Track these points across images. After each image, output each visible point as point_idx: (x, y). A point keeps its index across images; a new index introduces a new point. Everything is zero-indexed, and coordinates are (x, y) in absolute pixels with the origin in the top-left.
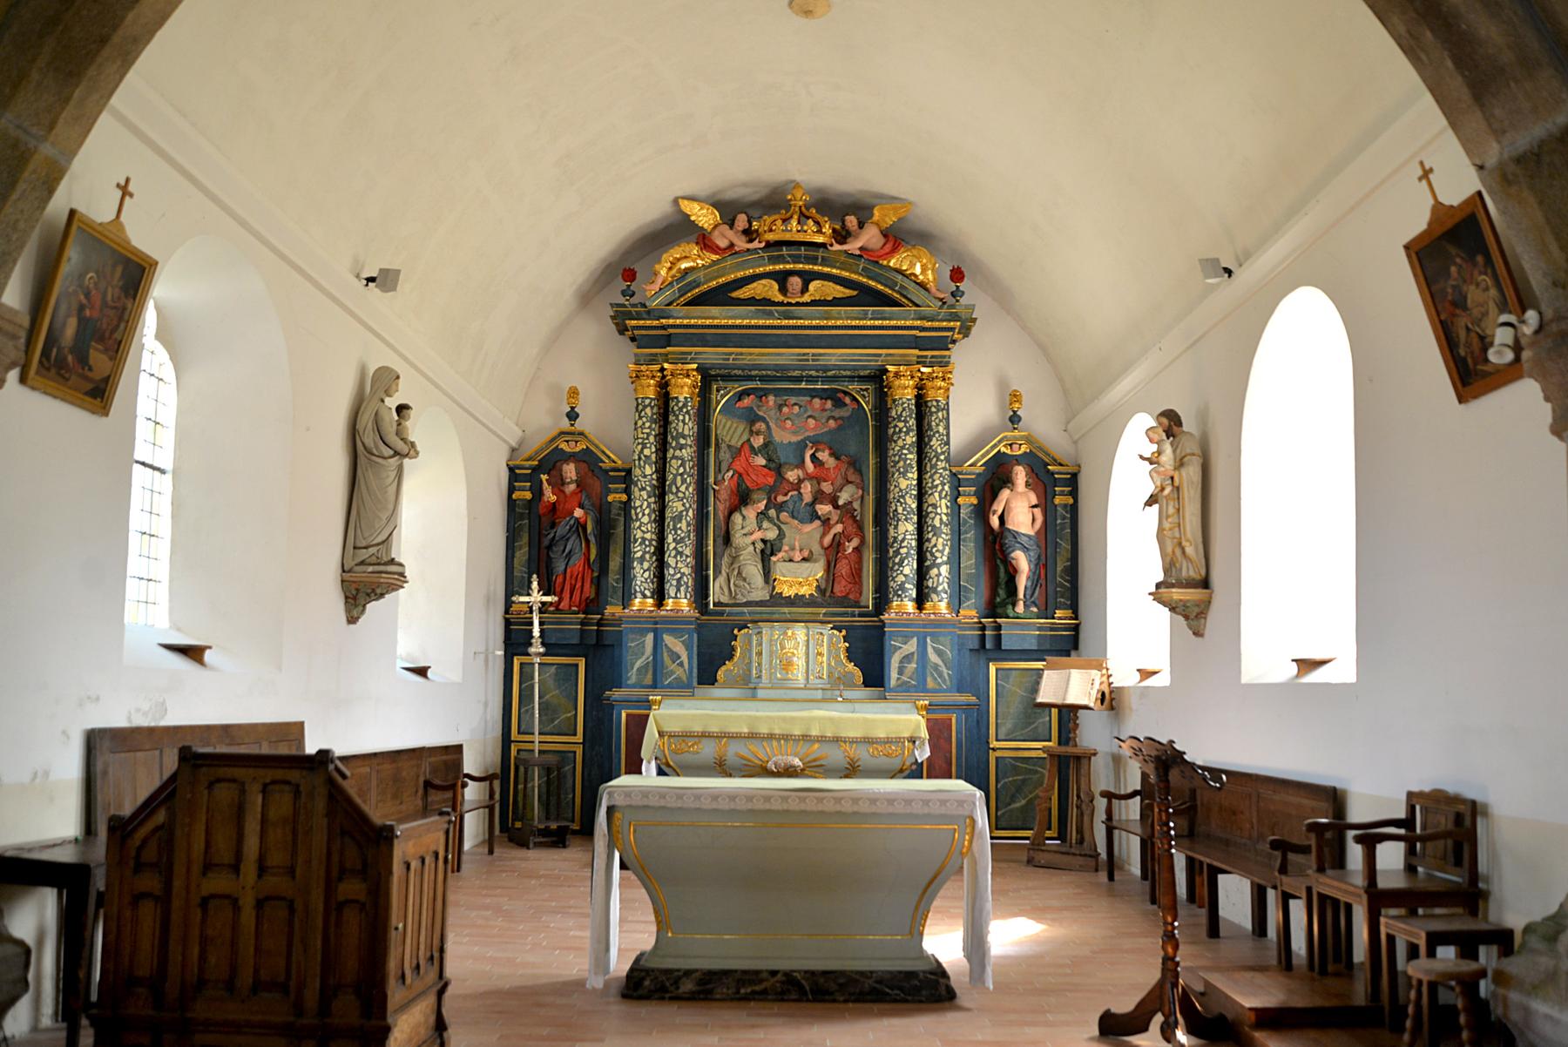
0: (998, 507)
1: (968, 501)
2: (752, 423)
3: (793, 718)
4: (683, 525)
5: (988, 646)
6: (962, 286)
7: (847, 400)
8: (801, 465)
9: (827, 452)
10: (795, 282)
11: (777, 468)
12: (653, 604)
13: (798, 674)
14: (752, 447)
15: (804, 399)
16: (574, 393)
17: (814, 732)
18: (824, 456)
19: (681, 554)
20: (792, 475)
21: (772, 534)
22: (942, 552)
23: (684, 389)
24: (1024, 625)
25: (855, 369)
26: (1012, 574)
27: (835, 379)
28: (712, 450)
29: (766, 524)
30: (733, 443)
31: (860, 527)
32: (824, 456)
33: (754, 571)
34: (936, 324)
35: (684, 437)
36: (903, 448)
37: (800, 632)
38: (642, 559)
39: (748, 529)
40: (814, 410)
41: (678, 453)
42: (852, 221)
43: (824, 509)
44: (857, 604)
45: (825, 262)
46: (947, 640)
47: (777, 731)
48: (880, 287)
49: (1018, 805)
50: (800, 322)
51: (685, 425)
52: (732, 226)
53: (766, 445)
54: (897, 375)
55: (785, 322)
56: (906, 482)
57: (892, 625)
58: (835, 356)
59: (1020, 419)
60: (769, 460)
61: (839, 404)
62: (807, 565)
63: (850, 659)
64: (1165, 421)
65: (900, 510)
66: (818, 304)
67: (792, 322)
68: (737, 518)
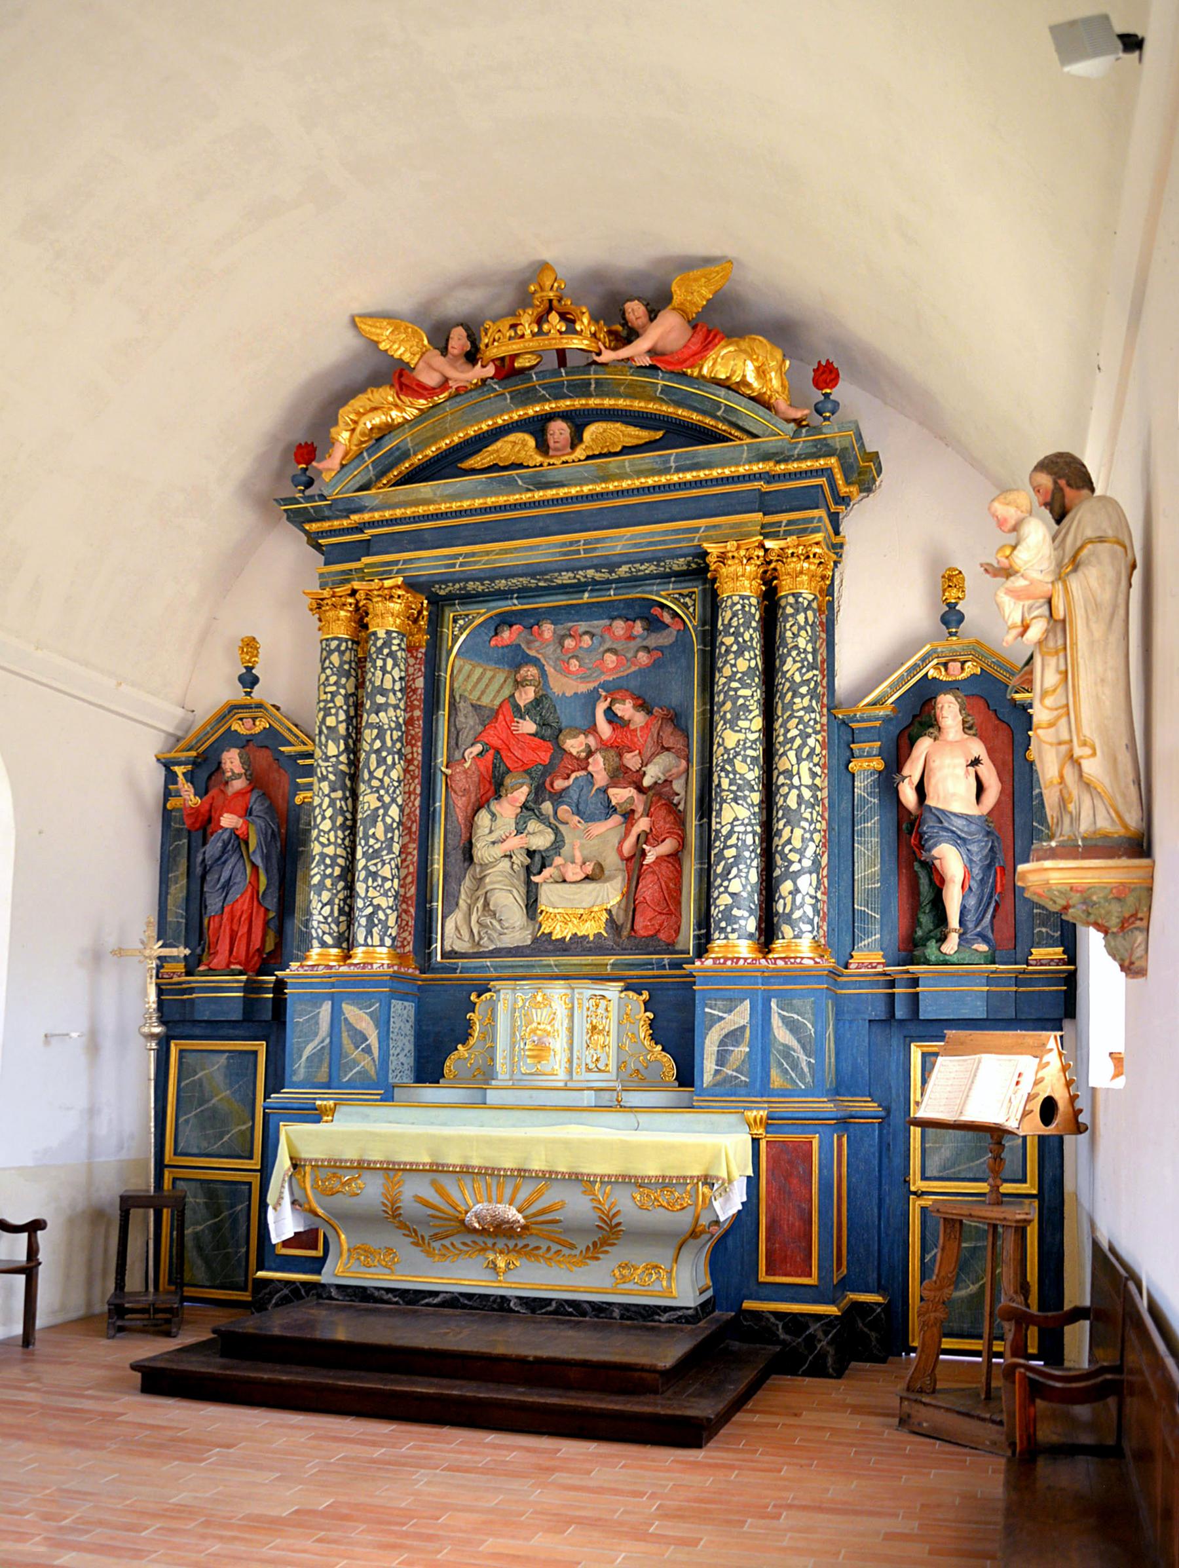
0: (913, 770)
1: (867, 767)
2: (517, 667)
3: (502, 1140)
4: (379, 830)
5: (899, 1014)
6: (836, 393)
7: (667, 618)
8: (592, 729)
9: (629, 704)
10: (559, 430)
11: (551, 732)
12: (343, 954)
13: (556, 1065)
14: (517, 706)
15: (600, 624)
16: (250, 645)
17: (537, 1165)
18: (625, 709)
19: (374, 875)
20: (575, 745)
21: (541, 840)
22: (801, 852)
23: (388, 618)
24: (960, 969)
25: (656, 559)
26: (938, 884)
27: (635, 580)
28: (444, 713)
29: (533, 825)
30: (485, 701)
31: (680, 820)
32: (625, 709)
33: (508, 901)
34: (793, 466)
35: (383, 692)
36: (731, 679)
37: (557, 992)
38: (321, 886)
39: (500, 833)
40: (616, 639)
41: (373, 718)
42: (635, 311)
43: (621, 795)
44: (670, 948)
45: (603, 389)
46: (807, 1004)
47: (476, 1162)
48: (696, 417)
49: (963, 1293)
50: (562, 492)
51: (388, 675)
52: (444, 351)
53: (538, 701)
54: (722, 558)
55: (538, 495)
56: (740, 735)
57: (707, 980)
58: (620, 541)
59: (961, 618)
60: (544, 724)
61: (654, 625)
62: (590, 886)
63: (655, 1038)
64: (1046, 480)
65: (725, 783)
66: (598, 462)
67: (551, 493)
68: (483, 818)
